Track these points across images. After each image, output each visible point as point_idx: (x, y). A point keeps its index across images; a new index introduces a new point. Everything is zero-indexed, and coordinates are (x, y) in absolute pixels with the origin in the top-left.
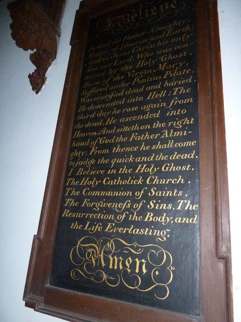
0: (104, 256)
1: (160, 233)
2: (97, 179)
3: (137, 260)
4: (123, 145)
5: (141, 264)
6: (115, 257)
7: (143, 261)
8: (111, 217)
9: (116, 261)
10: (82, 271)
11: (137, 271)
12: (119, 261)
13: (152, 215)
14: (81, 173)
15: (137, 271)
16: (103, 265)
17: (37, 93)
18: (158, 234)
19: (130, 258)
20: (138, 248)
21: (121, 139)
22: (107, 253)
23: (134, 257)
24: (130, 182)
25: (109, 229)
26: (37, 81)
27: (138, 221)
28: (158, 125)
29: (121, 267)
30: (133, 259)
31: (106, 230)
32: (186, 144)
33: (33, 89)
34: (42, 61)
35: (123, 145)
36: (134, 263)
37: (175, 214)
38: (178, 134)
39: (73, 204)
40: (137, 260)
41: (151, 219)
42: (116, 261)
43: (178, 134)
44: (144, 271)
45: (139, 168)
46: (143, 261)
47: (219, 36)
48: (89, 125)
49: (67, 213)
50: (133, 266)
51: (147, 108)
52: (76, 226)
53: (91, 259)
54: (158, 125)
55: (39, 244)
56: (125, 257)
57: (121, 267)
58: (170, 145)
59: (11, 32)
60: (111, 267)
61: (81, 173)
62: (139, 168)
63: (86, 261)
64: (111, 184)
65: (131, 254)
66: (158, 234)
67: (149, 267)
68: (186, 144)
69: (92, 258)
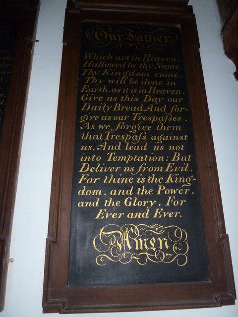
0: (130, 239)
1: (185, 179)
3: (159, 239)
5: (163, 242)
6: (140, 240)
9: (141, 244)
10: (110, 256)
11: (161, 247)
12: (144, 242)
13: (179, 154)
15: (161, 247)
18: (183, 181)
19: (153, 239)
24: (99, 169)
29: (146, 247)
32: (121, 158)
40: (159, 239)
41: (178, 159)
42: (141, 244)
44: (167, 247)
45: (86, 63)
47: (197, 31)
53: (116, 244)
56: (150, 238)
62: (86, 63)
64: (97, 138)
65: (154, 235)
66: (183, 181)
68: (121, 158)
69: (118, 243)
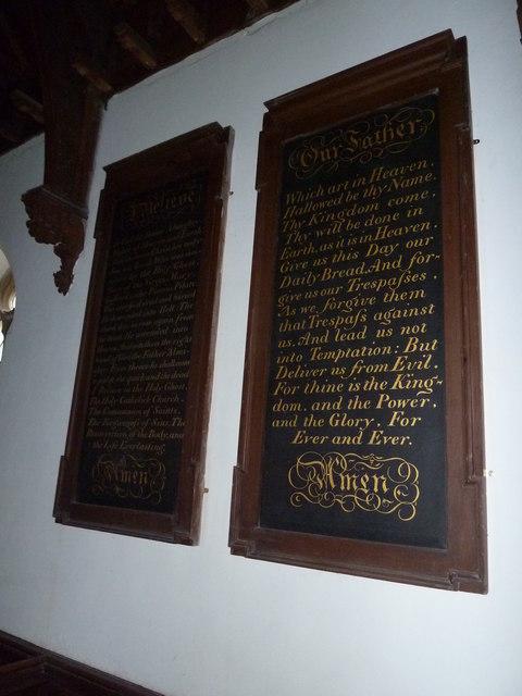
2: (116, 398)
3: (375, 477)
4: (137, 362)
5: (380, 482)
7: (382, 477)
8: (125, 435)
11: (376, 490)
14: (415, 348)
15: (376, 490)
16: (333, 486)
17: (65, 294)
20: (375, 462)
21: (136, 356)
22: (337, 468)
23: (371, 473)
25: (375, 441)
26: (63, 281)
27: (318, 427)
28: (166, 342)
29: (355, 487)
30: (370, 476)
31: (371, 442)
33: (59, 291)
34: (68, 255)
35: (137, 362)
36: (372, 480)
37: (168, 430)
38: (179, 352)
39: (96, 424)
40: (375, 477)
43: (179, 352)
44: (385, 490)
46: (382, 477)
48: (110, 339)
49: (91, 433)
50: (370, 485)
51: (159, 322)
52: (97, 445)
53: (315, 479)
54: (166, 342)
55: (66, 463)
56: (361, 474)
57: (355, 487)
58: (173, 364)
59: (27, 218)
60: (343, 488)
61: (415, 348)
63: (310, 482)
67: (149, 479)
